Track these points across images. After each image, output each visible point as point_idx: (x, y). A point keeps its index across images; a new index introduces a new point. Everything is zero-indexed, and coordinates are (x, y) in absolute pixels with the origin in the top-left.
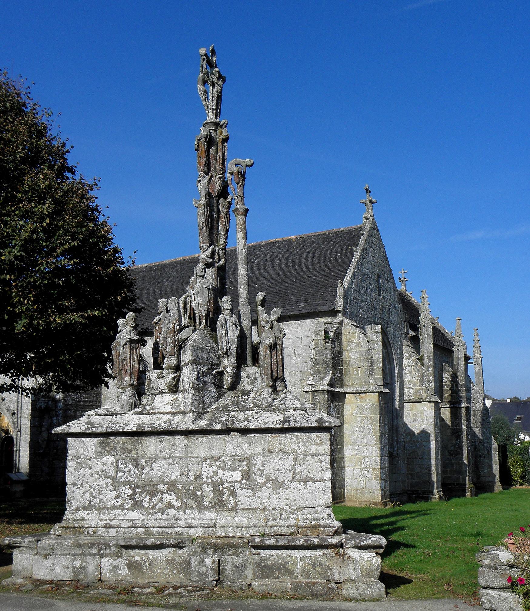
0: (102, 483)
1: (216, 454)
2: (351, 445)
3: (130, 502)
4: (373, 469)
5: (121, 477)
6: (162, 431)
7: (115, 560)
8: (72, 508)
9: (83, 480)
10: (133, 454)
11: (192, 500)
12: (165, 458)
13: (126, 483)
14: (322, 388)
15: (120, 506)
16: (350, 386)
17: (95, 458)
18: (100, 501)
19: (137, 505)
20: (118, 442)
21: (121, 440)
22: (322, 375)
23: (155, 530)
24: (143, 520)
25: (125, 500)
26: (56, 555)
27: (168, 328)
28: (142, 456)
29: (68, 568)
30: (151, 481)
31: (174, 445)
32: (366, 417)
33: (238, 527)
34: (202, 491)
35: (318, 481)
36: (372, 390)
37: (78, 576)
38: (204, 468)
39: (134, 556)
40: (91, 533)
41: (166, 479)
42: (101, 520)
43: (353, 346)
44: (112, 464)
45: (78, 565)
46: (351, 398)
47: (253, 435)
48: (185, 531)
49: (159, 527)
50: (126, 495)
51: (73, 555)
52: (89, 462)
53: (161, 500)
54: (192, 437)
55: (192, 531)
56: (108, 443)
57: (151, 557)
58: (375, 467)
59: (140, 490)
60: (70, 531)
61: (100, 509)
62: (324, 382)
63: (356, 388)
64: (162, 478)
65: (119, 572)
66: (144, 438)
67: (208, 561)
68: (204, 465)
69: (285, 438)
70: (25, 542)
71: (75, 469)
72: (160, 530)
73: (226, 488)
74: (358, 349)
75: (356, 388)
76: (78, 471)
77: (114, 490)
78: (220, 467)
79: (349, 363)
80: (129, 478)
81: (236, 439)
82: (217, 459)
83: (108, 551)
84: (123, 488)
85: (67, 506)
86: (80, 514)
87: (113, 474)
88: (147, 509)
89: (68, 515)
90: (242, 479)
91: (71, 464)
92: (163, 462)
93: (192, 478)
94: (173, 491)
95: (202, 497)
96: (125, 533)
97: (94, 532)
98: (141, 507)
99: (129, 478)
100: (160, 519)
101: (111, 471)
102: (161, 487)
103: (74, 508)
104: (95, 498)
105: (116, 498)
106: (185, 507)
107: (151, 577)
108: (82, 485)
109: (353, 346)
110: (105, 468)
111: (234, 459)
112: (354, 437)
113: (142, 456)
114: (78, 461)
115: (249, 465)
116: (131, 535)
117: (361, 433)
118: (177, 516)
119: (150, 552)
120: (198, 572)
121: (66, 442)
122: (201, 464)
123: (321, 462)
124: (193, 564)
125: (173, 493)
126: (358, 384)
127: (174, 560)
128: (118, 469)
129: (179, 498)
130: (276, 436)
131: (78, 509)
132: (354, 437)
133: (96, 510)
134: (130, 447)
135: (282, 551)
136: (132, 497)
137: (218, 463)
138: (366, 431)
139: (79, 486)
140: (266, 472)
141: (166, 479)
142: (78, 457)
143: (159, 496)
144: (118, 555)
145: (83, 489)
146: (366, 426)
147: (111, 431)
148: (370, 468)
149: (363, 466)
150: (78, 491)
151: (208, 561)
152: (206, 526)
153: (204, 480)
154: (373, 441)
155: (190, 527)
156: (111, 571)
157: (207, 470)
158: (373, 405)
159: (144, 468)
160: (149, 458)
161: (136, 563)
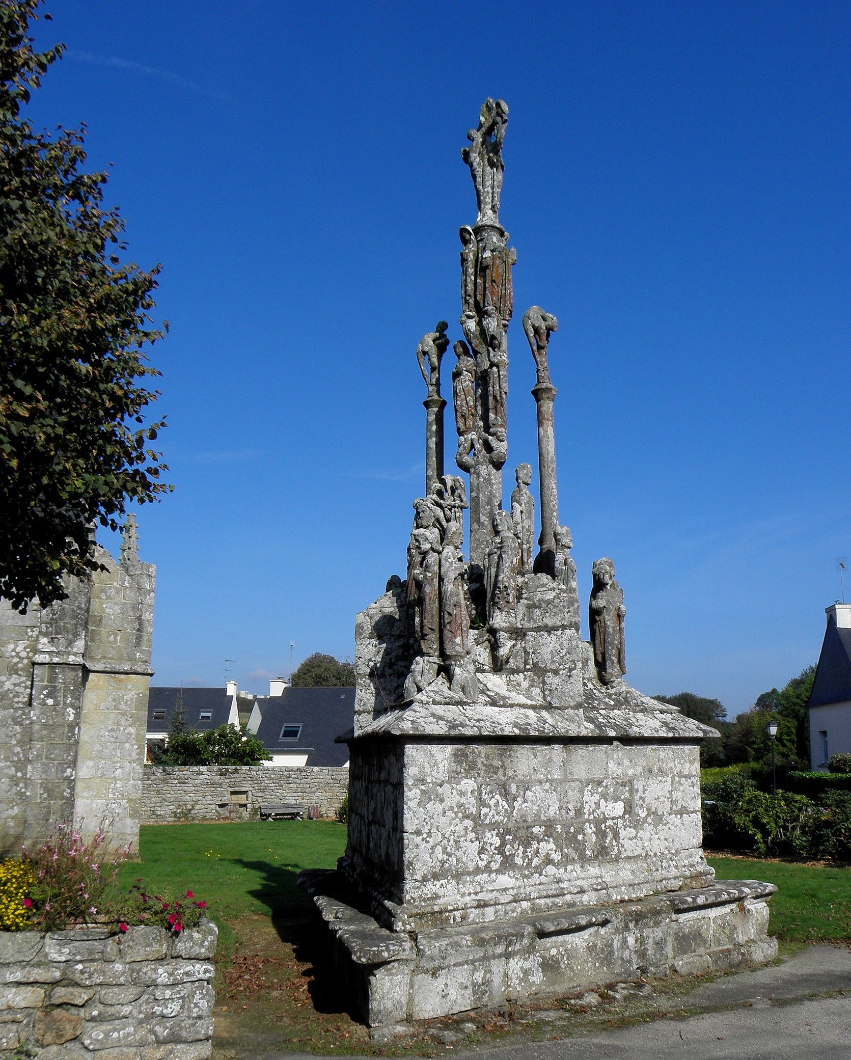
0: (460, 828)
1: (598, 775)
2: (91, 759)
3: (499, 858)
4: (130, 800)
5: (486, 815)
6: (550, 737)
7: (526, 959)
8: (415, 877)
9: (432, 824)
10: (500, 773)
11: (573, 848)
12: (540, 782)
13: (493, 826)
14: (71, 659)
15: (486, 866)
16: (99, 660)
17: (449, 782)
18: (458, 860)
19: (508, 864)
20: (480, 753)
21: (482, 749)
22: (71, 636)
23: (542, 901)
24: (519, 887)
25: (492, 857)
26: (449, 967)
27: (584, 834)
28: (512, 778)
29: (466, 987)
30: (524, 821)
31: (550, 760)
32: (123, 714)
33: (630, 885)
34: (584, 834)
35: (692, 812)
36: (140, 670)
37: (480, 999)
38: (586, 798)
39: (549, 949)
40: (458, 919)
41: (543, 818)
42: (463, 895)
43: (113, 592)
44: (472, 792)
45: (480, 981)
46: (99, 680)
47: (591, 748)
48: (577, 898)
49: (545, 897)
50: (493, 847)
51: (473, 962)
52: (440, 790)
53: (537, 852)
54: (572, 747)
55: (585, 898)
56: (466, 756)
57: (569, 947)
58: (133, 796)
59: (511, 837)
60: (427, 922)
61: (458, 876)
62: (75, 650)
63: (110, 664)
64: (538, 815)
65: (531, 979)
66: (515, 747)
67: (631, 940)
68: (586, 792)
69: (665, 752)
70: (404, 950)
71: (419, 805)
72: (548, 901)
73: (609, 827)
74: (120, 598)
75: (110, 664)
76: (424, 808)
77: (477, 839)
78: (604, 796)
79: (101, 620)
80: (497, 817)
81: (619, 752)
82: (599, 783)
83: (518, 947)
84: (488, 834)
85: (407, 875)
86: (431, 888)
87: (474, 811)
88: (521, 868)
89: (411, 890)
90: (625, 813)
91: (412, 795)
92: (538, 788)
93: (572, 814)
94: (551, 836)
95: (584, 841)
96: (506, 913)
97: (463, 918)
98: (514, 866)
99: (497, 817)
100: (539, 884)
101: (471, 804)
102: (536, 830)
103: (418, 877)
104: (450, 855)
105: (479, 853)
106: (566, 861)
107: (571, 979)
108: (429, 834)
109: (113, 592)
110: (463, 800)
111: (617, 782)
112: (98, 747)
113: (512, 778)
114: (423, 787)
115: (632, 791)
116: (515, 915)
117: (112, 739)
118: (558, 876)
119: (568, 938)
120: (622, 959)
121: (400, 755)
122: (581, 791)
123: (693, 786)
124: (616, 948)
125: (551, 840)
126: (115, 657)
127: (595, 945)
128: (481, 803)
129: (559, 847)
130: (655, 750)
131: (425, 879)
132: (98, 747)
133: (453, 877)
134: (497, 763)
135: (703, 911)
136: (500, 850)
137: (600, 790)
138: (122, 738)
139: (425, 836)
140: (647, 801)
141: (543, 818)
142: (423, 781)
143: (535, 845)
144: (530, 950)
145: (431, 843)
146: (122, 729)
147: (487, 733)
148: (123, 797)
149: (111, 796)
150: (423, 845)
151: (631, 940)
152: (599, 887)
153: (586, 817)
154: (134, 754)
155: (582, 891)
156: (521, 980)
157: (590, 799)
158: (138, 695)
159: (515, 799)
160: (521, 781)
161: (553, 961)
